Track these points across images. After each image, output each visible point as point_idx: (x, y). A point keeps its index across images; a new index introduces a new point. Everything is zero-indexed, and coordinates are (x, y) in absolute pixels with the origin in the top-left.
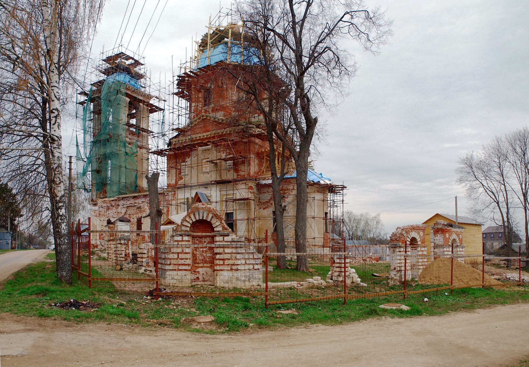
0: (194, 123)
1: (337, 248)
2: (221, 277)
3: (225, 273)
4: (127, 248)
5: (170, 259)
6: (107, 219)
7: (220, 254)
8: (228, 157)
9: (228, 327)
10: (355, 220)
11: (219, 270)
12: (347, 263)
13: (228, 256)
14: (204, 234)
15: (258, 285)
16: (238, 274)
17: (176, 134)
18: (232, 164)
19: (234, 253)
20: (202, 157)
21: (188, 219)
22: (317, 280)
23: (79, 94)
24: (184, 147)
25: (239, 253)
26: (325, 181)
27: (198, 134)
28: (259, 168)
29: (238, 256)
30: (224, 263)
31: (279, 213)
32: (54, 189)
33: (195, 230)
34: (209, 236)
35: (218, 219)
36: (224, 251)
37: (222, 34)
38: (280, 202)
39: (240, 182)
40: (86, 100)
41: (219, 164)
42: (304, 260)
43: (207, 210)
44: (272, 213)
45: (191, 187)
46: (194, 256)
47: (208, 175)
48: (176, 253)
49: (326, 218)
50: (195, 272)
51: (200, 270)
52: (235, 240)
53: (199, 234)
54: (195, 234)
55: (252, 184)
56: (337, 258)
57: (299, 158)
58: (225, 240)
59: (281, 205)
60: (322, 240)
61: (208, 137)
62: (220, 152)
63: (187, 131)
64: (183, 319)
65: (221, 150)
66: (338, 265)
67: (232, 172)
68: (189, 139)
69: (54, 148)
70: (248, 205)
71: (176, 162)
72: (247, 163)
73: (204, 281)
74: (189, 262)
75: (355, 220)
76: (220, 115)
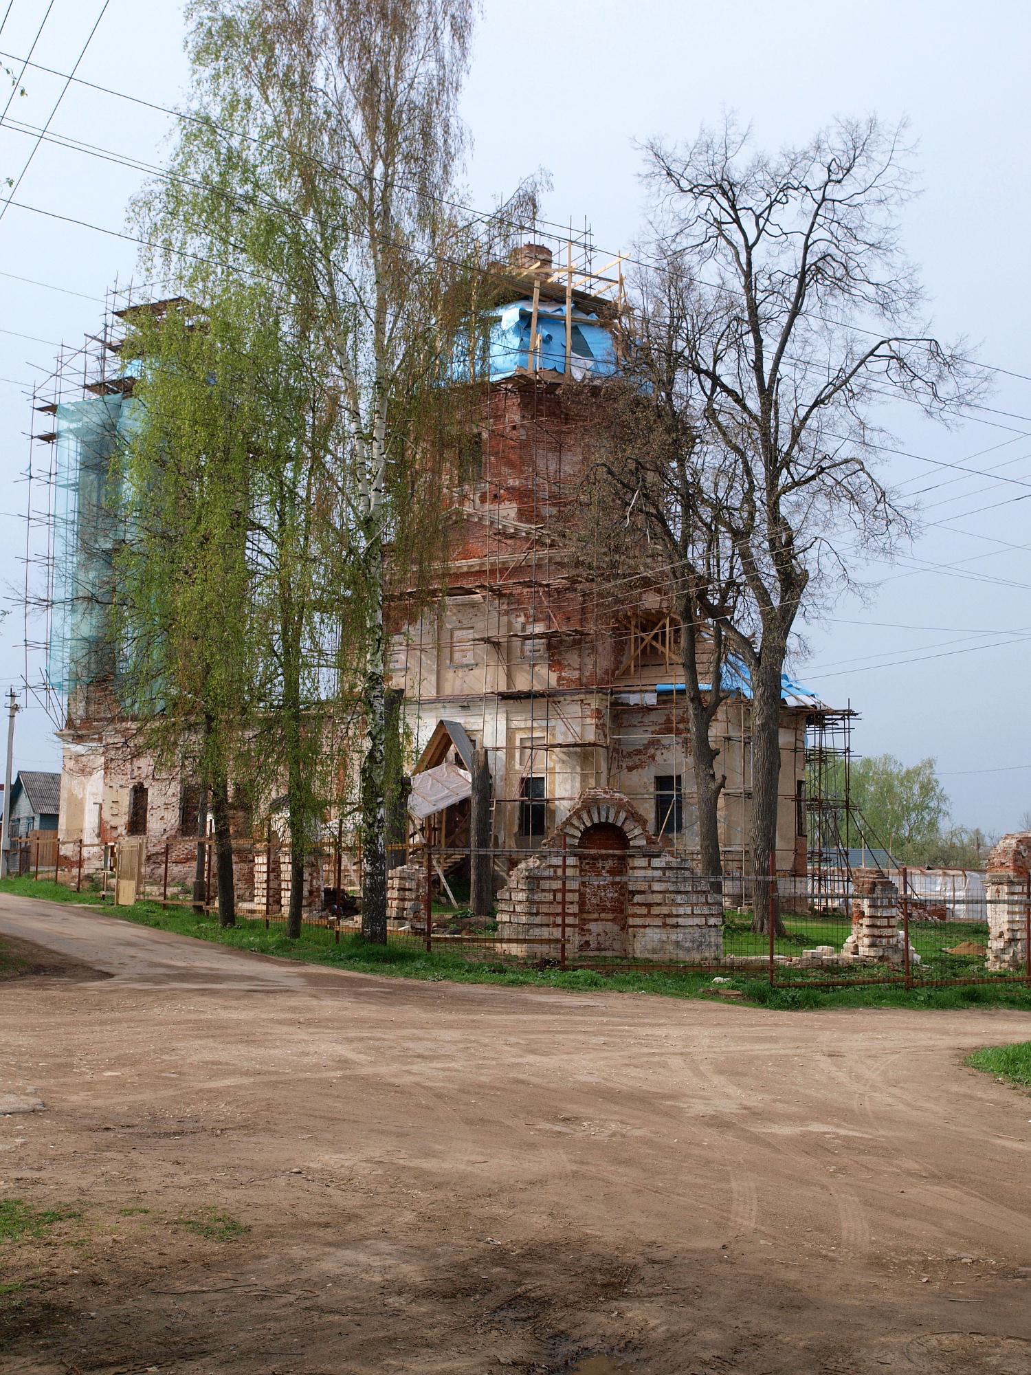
4: (315, 874)
13: (657, 898)
14: (604, 852)
18: (542, 648)
19: (670, 892)
21: (575, 822)
23: (41, 409)
26: (799, 697)
29: (679, 899)
30: (649, 911)
34: (614, 856)
36: (650, 887)
39: (568, 698)
44: (653, 780)
48: (549, 891)
50: (583, 930)
51: (592, 926)
52: (674, 865)
53: (593, 851)
54: (586, 851)
59: (713, 776)
73: (598, 949)
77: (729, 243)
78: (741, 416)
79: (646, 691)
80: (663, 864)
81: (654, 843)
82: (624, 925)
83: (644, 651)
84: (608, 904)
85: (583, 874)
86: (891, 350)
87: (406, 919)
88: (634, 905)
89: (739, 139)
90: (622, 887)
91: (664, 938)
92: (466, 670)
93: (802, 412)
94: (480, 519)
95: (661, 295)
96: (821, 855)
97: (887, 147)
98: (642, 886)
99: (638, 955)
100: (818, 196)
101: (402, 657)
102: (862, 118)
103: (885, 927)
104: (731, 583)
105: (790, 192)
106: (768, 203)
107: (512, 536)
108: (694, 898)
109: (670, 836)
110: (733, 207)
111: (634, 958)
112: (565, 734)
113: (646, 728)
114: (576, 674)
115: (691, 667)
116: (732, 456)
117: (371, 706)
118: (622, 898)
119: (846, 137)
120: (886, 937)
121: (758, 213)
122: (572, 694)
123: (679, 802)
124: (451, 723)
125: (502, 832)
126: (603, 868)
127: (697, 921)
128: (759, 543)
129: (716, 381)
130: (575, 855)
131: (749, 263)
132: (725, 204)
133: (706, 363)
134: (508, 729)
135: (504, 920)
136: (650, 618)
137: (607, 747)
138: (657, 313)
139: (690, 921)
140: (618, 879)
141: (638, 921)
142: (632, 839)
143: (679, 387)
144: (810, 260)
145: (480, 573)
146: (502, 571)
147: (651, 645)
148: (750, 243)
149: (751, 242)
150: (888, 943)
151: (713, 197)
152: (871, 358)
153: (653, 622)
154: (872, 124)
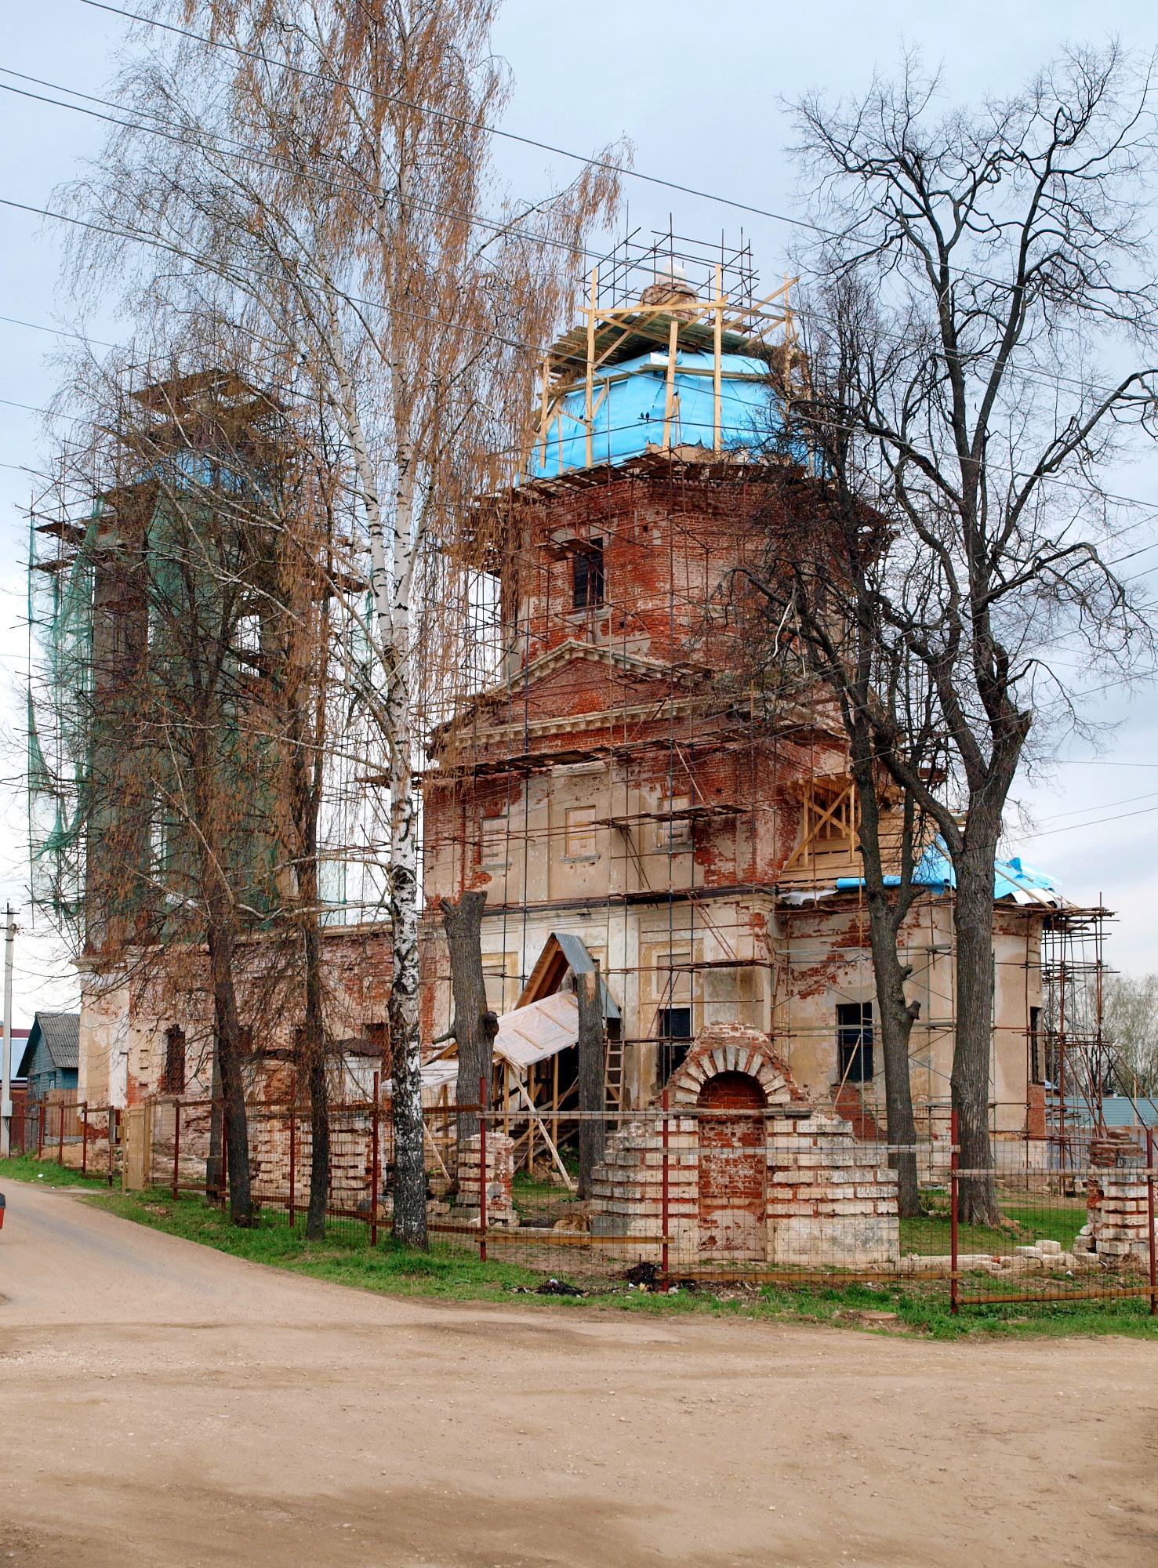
0: (537, 674)
1: (1111, 1150)
6: (164, 1026)
7: (786, 1169)
8: (666, 808)
9: (931, 1330)
10: (1120, 1002)
12: (655, 1200)
13: (806, 1176)
14: (733, 1112)
15: (889, 1261)
16: (832, 1228)
18: (685, 831)
19: (824, 1168)
22: (1046, 1251)
23: (42, 529)
25: (837, 1168)
26: (1031, 891)
29: (837, 1177)
30: (795, 1195)
31: (897, 1028)
32: (400, 1005)
34: (747, 1117)
36: (796, 1160)
37: (637, 332)
38: (900, 990)
39: (720, 899)
40: (72, 557)
41: (634, 829)
42: (983, 1189)
43: (748, 1045)
44: (834, 1010)
46: (704, 1174)
47: (592, 870)
49: (1032, 1032)
50: (706, 1221)
51: (717, 1215)
52: (828, 1130)
53: (718, 1112)
54: (707, 1111)
55: (762, 906)
56: (1111, 1184)
57: (965, 845)
59: (902, 1002)
60: (1023, 1110)
61: (592, 727)
62: (638, 786)
63: (506, 704)
64: (838, 1312)
65: (644, 776)
66: (1112, 1205)
67: (686, 860)
68: (516, 733)
69: (402, 900)
70: (748, 981)
71: (464, 817)
72: (744, 827)
73: (728, 1248)
74: (693, 1192)
75: (1120, 1002)
76: (639, 651)
77: (919, 244)
78: (937, 494)
80: (814, 1129)
81: (800, 1099)
83: (823, 828)
84: (740, 1185)
85: (706, 1143)
86: (1144, 387)
88: (774, 1185)
89: (925, 88)
91: (816, 1232)
93: (1021, 483)
94: (602, 657)
95: (827, 327)
96: (1063, 1110)
97: (1139, 84)
98: (783, 1160)
99: (780, 1257)
100: (1041, 167)
101: (501, 848)
102: (1101, 47)
103: (1132, 1213)
104: (927, 730)
105: (1004, 164)
106: (969, 183)
109: (857, 1085)
110: (921, 190)
113: (824, 939)
115: (870, 851)
116: (927, 551)
117: (399, 913)
119: (1075, 71)
120: (1133, 1227)
121: (957, 198)
125: (635, 1085)
126: (733, 1134)
127: (860, 1207)
128: (964, 670)
129: (907, 452)
130: (694, 1118)
131: (945, 272)
132: (911, 188)
133: (893, 423)
136: (830, 787)
137: (771, 966)
138: (822, 353)
139: (850, 1208)
140: (750, 1151)
141: (780, 1209)
143: (855, 456)
144: (1029, 265)
145: (601, 731)
146: (630, 727)
148: (946, 243)
149: (946, 242)
150: (1138, 1235)
151: (891, 176)
152: (1119, 402)
154: (1115, 54)
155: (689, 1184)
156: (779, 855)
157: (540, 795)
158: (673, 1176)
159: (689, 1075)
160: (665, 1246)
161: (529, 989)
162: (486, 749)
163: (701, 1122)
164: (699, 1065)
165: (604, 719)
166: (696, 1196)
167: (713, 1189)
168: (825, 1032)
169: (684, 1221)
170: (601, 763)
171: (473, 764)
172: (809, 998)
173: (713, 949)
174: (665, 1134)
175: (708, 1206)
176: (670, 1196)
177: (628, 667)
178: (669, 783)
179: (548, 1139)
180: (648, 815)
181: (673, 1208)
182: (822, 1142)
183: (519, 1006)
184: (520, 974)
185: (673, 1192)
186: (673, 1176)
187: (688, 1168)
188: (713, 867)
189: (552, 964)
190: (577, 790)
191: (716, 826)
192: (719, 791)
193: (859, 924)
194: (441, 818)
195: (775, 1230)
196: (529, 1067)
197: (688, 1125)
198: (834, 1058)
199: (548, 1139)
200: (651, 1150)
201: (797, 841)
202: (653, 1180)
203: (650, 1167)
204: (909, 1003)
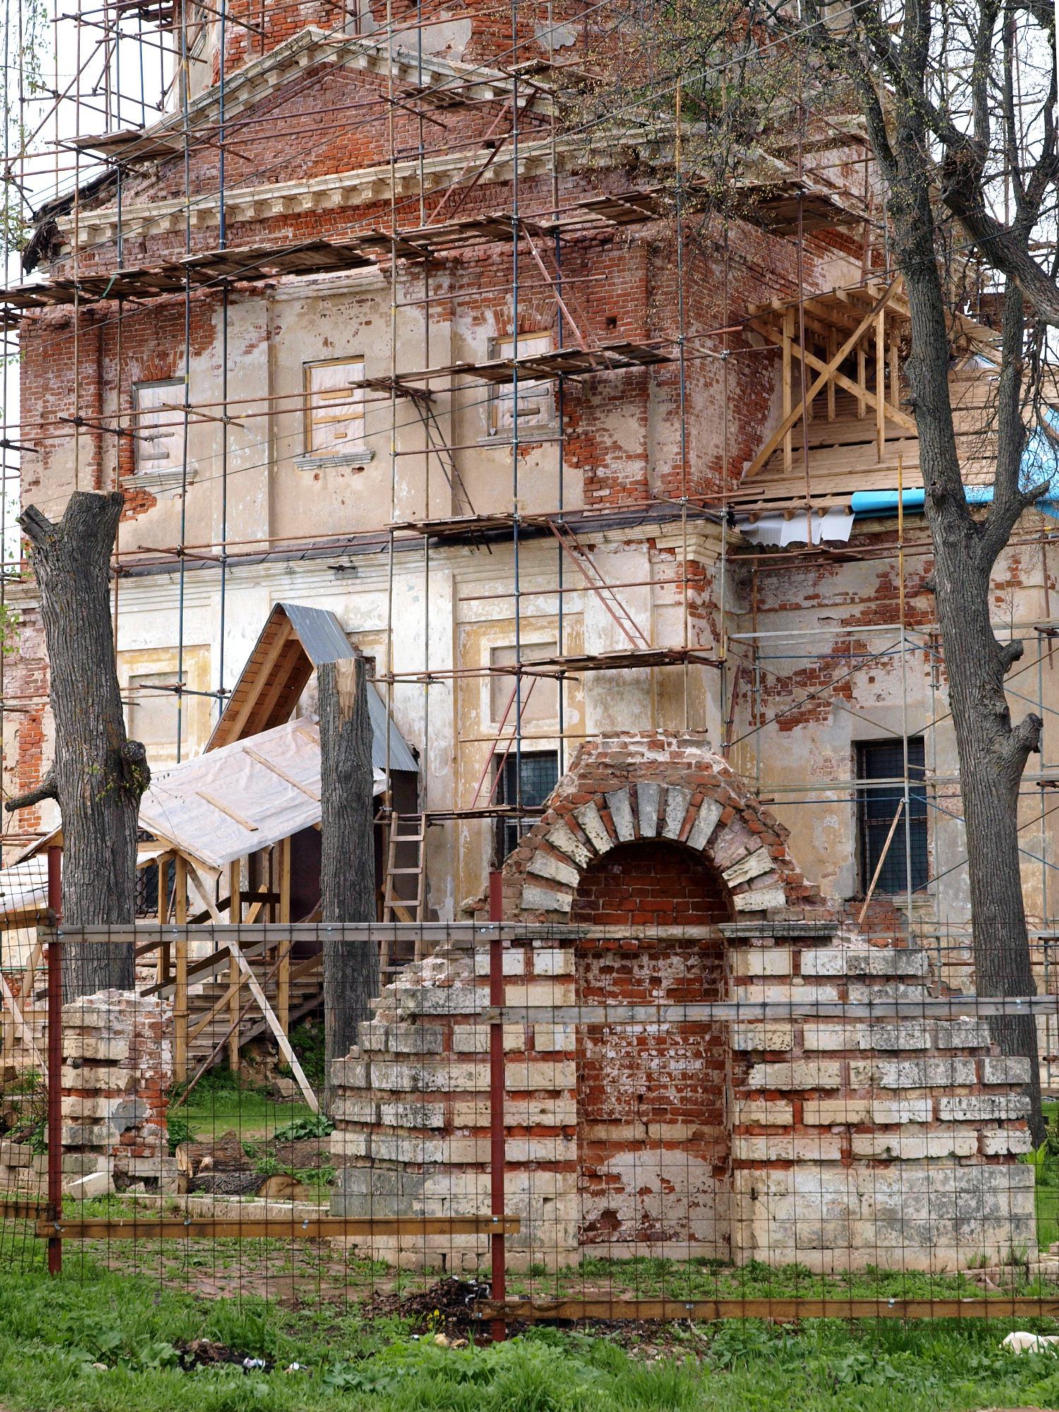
2: (783, 1209)
3: (804, 1179)
5: (449, 1096)
7: (776, 1057)
8: (507, 352)
11: (767, 1164)
12: (476, 1130)
13: (829, 1073)
14: (653, 931)
15: (1014, 1262)
17: (93, 169)
18: (546, 404)
20: (310, 347)
24: (171, 276)
27: (273, 176)
28: (742, 428)
29: (890, 1073)
30: (798, 1115)
33: (593, 905)
34: (687, 943)
35: (753, 833)
36: (799, 1038)
39: (615, 535)
43: (687, 781)
44: (847, 751)
45: (224, 562)
46: (589, 1071)
47: (357, 481)
50: (594, 1176)
51: (621, 1162)
52: (877, 968)
53: (620, 932)
54: (596, 932)
58: (807, 970)
59: (1004, 718)
61: (356, 201)
68: (203, 214)
71: (101, 383)
73: (647, 1237)
74: (565, 1112)
79: (824, 511)
81: (808, 900)
82: (725, 1159)
84: (672, 1094)
87: (97, 1149)
88: (749, 1095)
90: (716, 1041)
92: (347, 470)
94: (373, 61)
99: (761, 1256)
107: (455, 104)
108: (939, 1073)
109: (897, 900)
111: (754, 1266)
112: (606, 633)
113: (825, 613)
114: (635, 470)
118: (715, 1075)
122: (625, 523)
123: (919, 808)
124: (307, 611)
126: (656, 981)
127: (940, 1144)
130: (564, 944)
134: (457, 624)
135: (351, 1150)
136: (835, 316)
137: (720, 665)
140: (699, 1013)
141: (759, 1148)
142: (738, 889)
147: (840, 391)
153: (840, 330)
155: (555, 1094)
156: (734, 451)
157: (253, 335)
158: (516, 1075)
159: (552, 848)
160: (498, 1239)
161: (230, 716)
162: (143, 247)
163: (580, 954)
164: (576, 826)
165: (381, 183)
166: (572, 1120)
167: (611, 1104)
168: (830, 795)
169: (544, 1177)
170: (374, 269)
171: (114, 274)
172: (798, 730)
173: (606, 633)
174: (497, 981)
175: (600, 1143)
176: (509, 1120)
177: (426, 79)
178: (510, 308)
179: (270, 1016)
180: (470, 369)
181: (515, 1149)
182: (857, 993)
183: (209, 748)
184: (215, 688)
185: (515, 1113)
186: (516, 1075)
187: (552, 1056)
188: (601, 472)
189: (277, 667)
190: (325, 326)
191: (607, 391)
192: (612, 322)
193: (898, 582)
194: (54, 384)
195: (754, 1196)
196: (234, 865)
197: (552, 961)
198: (848, 846)
199: (270, 1016)
200: (466, 1017)
201: (770, 423)
202: (469, 1085)
203: (465, 1057)
204: (1016, 720)
